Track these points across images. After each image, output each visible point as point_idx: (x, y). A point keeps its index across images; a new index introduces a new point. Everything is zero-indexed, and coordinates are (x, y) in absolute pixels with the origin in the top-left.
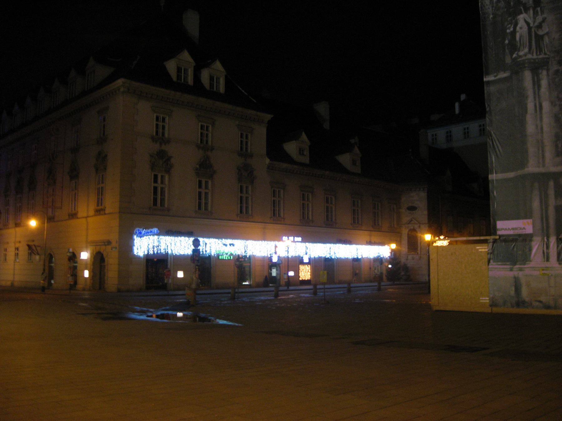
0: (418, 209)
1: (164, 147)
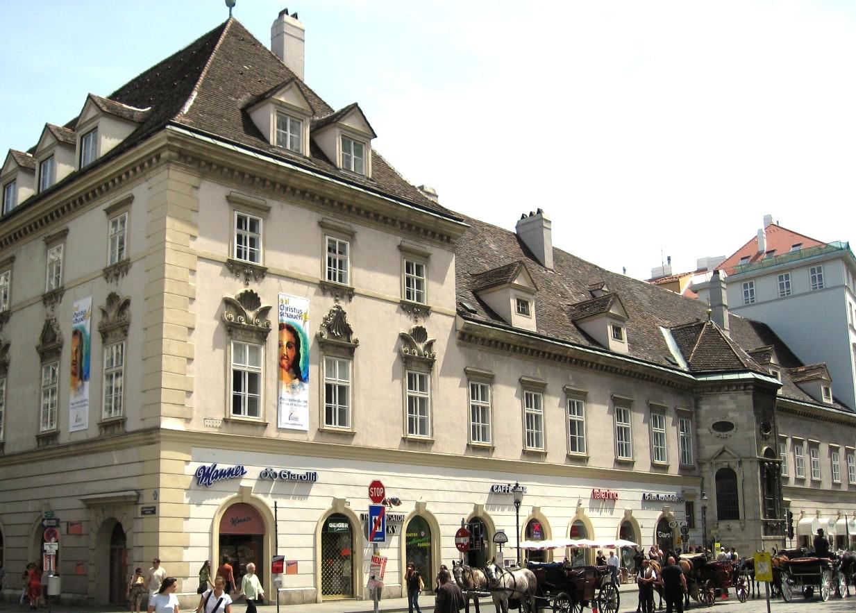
0: (734, 429)
1: (254, 287)
